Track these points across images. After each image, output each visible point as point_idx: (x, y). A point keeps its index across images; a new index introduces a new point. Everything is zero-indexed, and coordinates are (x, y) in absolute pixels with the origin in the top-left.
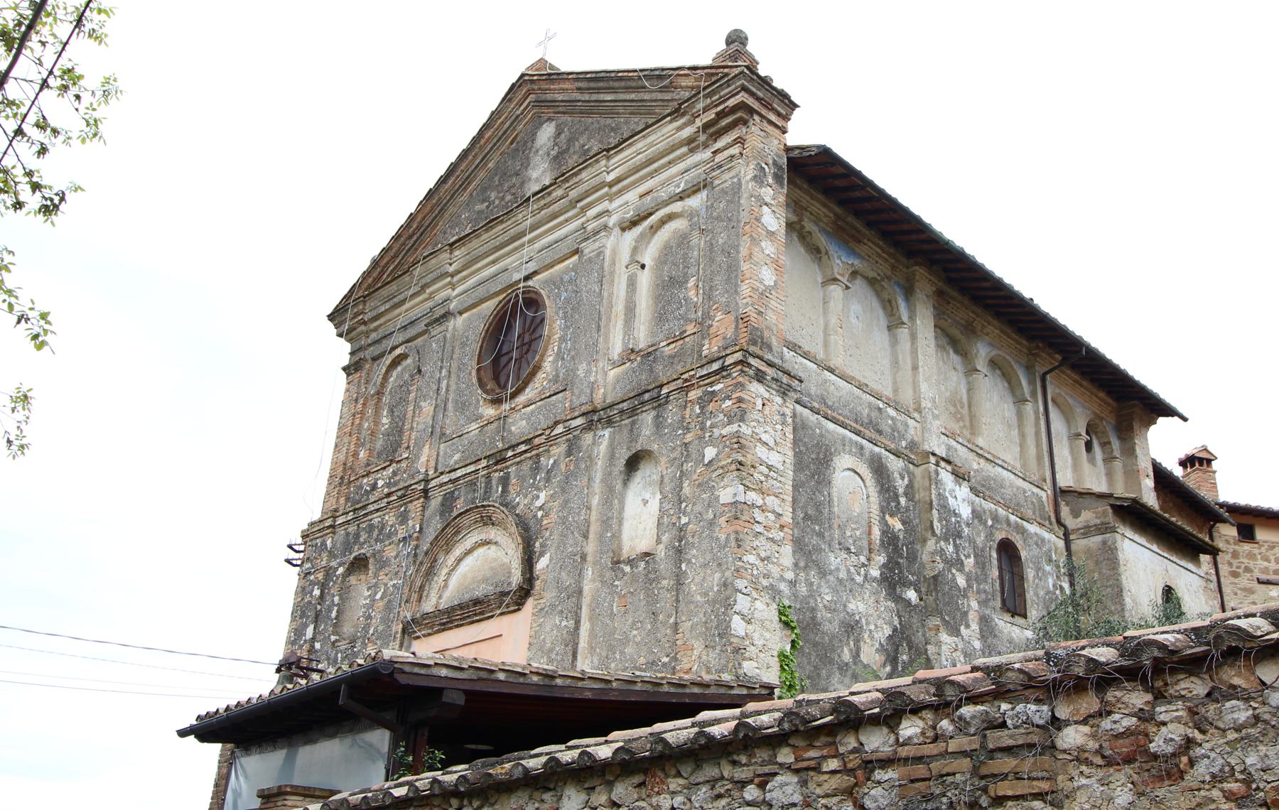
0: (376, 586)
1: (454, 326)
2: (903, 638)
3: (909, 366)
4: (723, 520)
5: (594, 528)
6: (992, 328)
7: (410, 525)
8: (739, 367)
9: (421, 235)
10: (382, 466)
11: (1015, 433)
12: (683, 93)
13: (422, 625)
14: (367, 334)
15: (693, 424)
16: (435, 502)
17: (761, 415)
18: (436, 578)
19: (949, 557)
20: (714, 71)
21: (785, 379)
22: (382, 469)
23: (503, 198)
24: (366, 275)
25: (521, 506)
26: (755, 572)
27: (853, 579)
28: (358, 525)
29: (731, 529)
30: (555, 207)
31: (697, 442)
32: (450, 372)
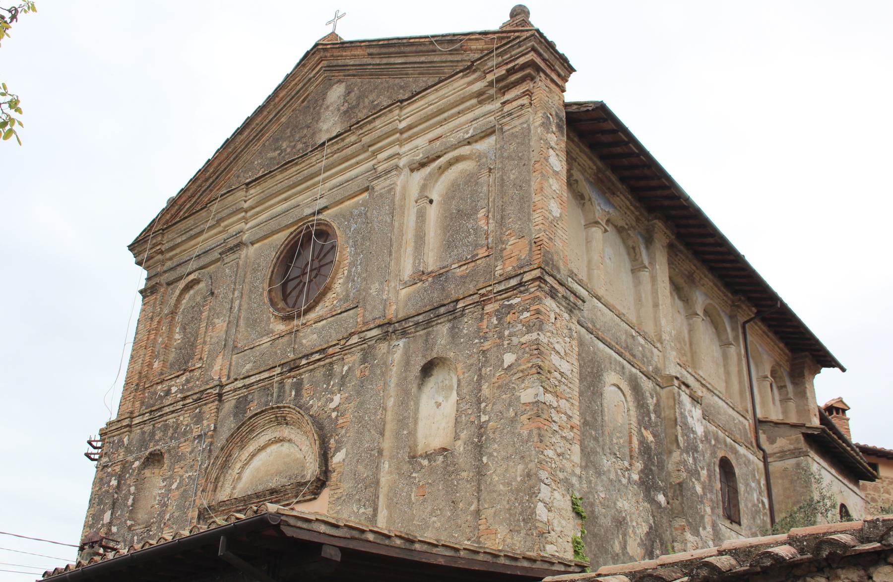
0: (171, 477)
1: (247, 254)
2: (656, 535)
3: (650, 304)
4: (524, 418)
5: (390, 427)
6: (708, 280)
7: (205, 425)
8: (537, 283)
9: (217, 178)
10: (176, 375)
11: (722, 370)
12: (472, 55)
13: (218, 511)
14: (163, 263)
15: (491, 334)
16: (229, 404)
17: (554, 327)
18: (230, 471)
19: (690, 468)
20: (505, 35)
21: (572, 298)
22: (175, 377)
23: (294, 147)
24: (164, 212)
25: (315, 408)
26: (553, 466)
27: (620, 481)
28: (154, 425)
29: (533, 426)
30: (348, 151)
31: (495, 349)
32: (242, 293)
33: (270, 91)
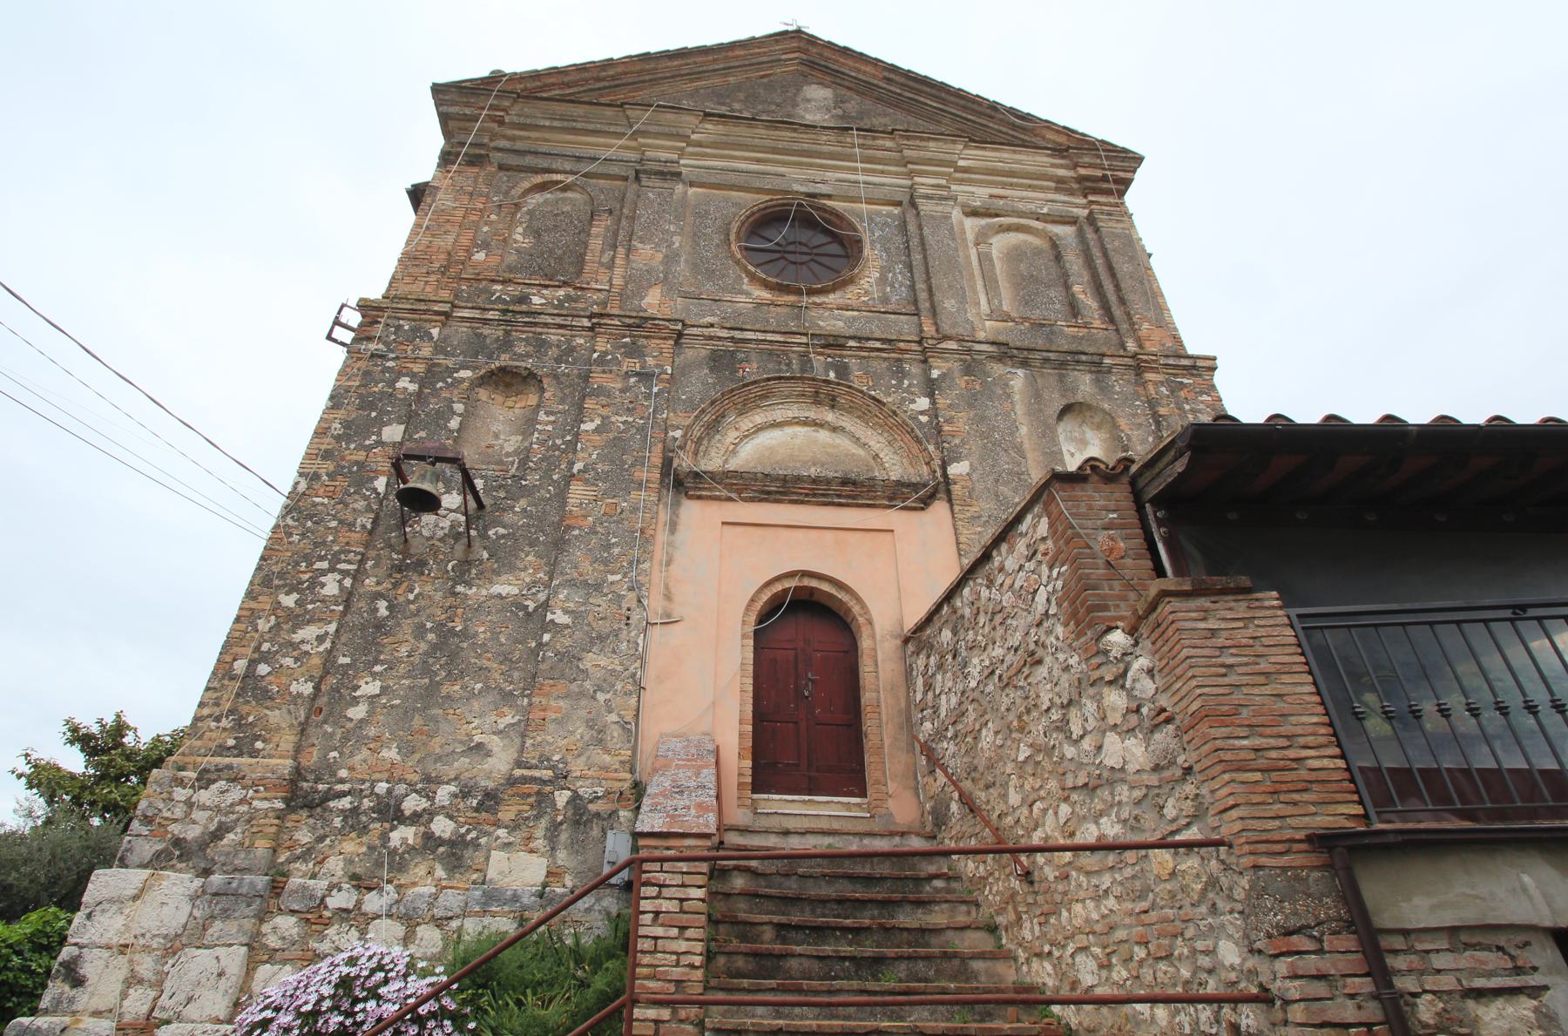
33: (726, 39)
